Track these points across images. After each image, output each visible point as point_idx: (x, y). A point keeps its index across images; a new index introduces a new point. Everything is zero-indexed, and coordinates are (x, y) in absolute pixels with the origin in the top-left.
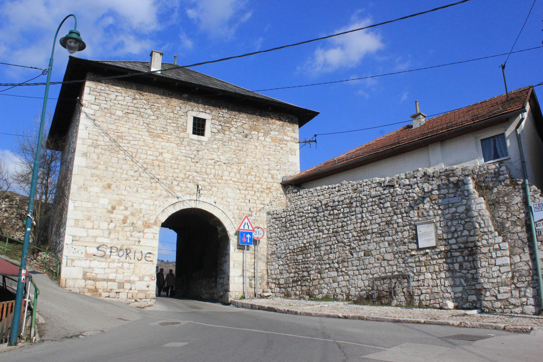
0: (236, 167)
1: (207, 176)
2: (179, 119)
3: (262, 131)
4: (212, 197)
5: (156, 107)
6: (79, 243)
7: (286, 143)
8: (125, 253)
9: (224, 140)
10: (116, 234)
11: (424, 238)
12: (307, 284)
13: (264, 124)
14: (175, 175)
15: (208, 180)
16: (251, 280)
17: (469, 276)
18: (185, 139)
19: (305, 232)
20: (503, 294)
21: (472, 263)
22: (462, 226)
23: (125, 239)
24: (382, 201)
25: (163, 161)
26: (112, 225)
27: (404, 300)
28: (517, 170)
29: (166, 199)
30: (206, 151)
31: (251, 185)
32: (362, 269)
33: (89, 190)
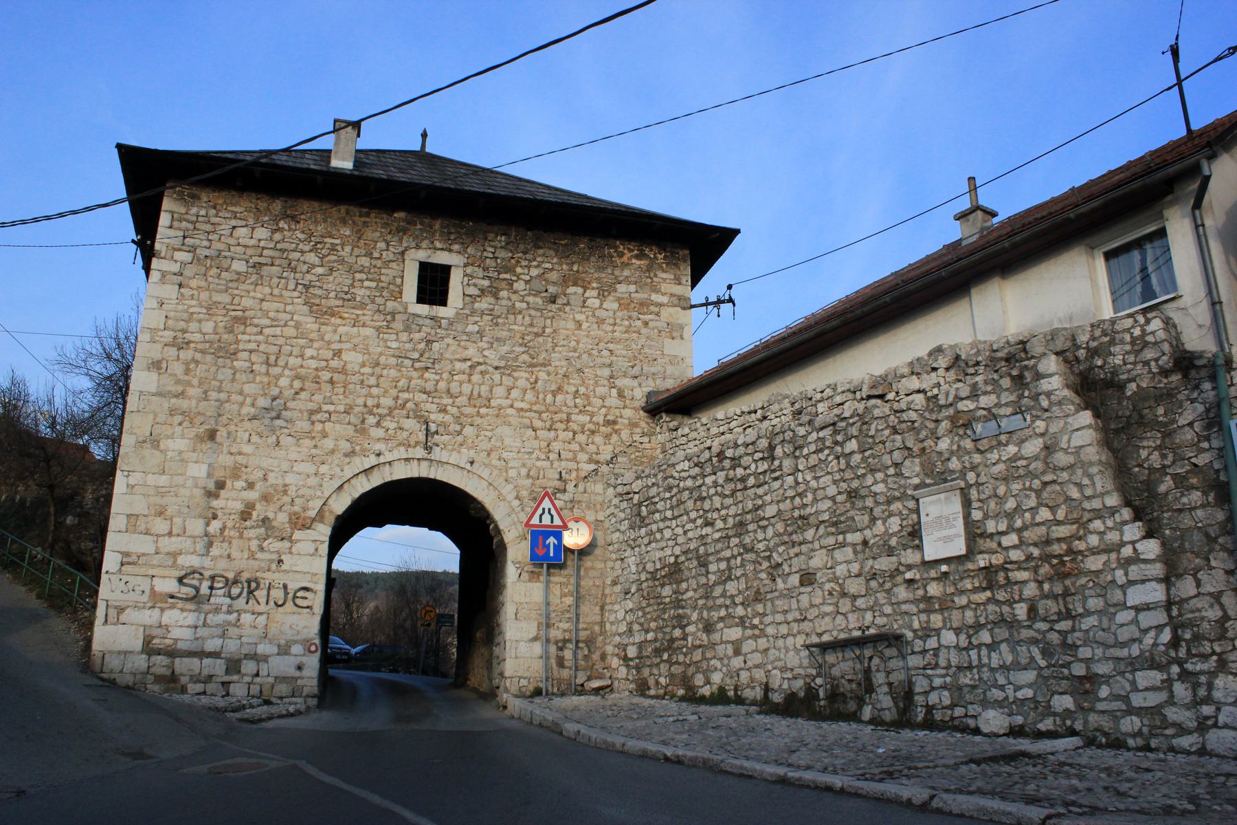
0: (525, 375)
1: (450, 401)
2: (383, 271)
3: (594, 285)
4: (464, 450)
5: (328, 246)
6: (135, 569)
7: (656, 309)
8: (246, 590)
9: (495, 313)
10: (226, 545)
11: (937, 535)
12: (681, 658)
13: (601, 269)
14: (370, 402)
15: (454, 410)
16: (561, 649)
17: (1054, 637)
18: (397, 316)
19: (677, 526)
20: (1146, 693)
21: (1061, 601)
22: (1033, 495)
23: (246, 556)
24: (839, 438)
25: (343, 371)
26: (215, 526)
27: (891, 704)
28: (1200, 326)
29: (347, 460)
30: (449, 340)
31: (564, 416)
32: (796, 621)
33: (162, 447)
